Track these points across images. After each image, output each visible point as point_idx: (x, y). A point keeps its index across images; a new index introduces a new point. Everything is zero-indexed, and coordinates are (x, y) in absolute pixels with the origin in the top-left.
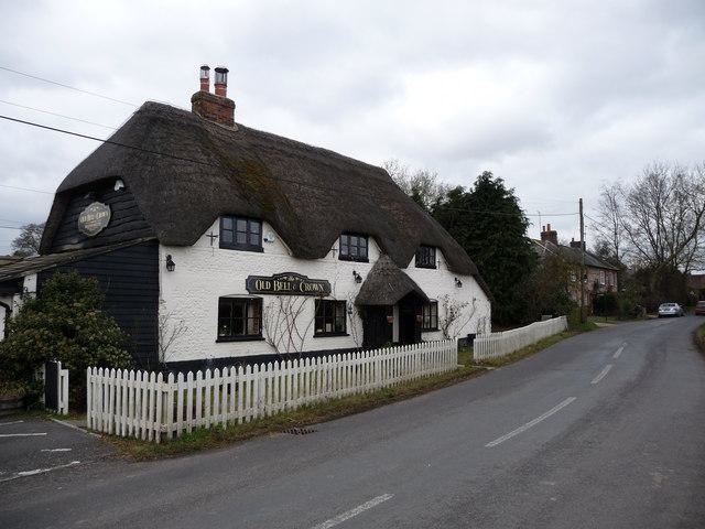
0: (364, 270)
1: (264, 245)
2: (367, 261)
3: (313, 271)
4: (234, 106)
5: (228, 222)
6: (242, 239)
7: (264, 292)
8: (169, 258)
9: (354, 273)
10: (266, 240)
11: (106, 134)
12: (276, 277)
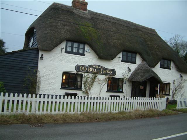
0: (133, 67)
1: (85, 53)
2: (135, 63)
3: (108, 65)
4: (87, 4)
5: (125, 53)
6: (166, 66)
7: (85, 72)
8: (42, 55)
9: (128, 68)
10: (86, 51)
11: (40, 14)
12: (90, 66)
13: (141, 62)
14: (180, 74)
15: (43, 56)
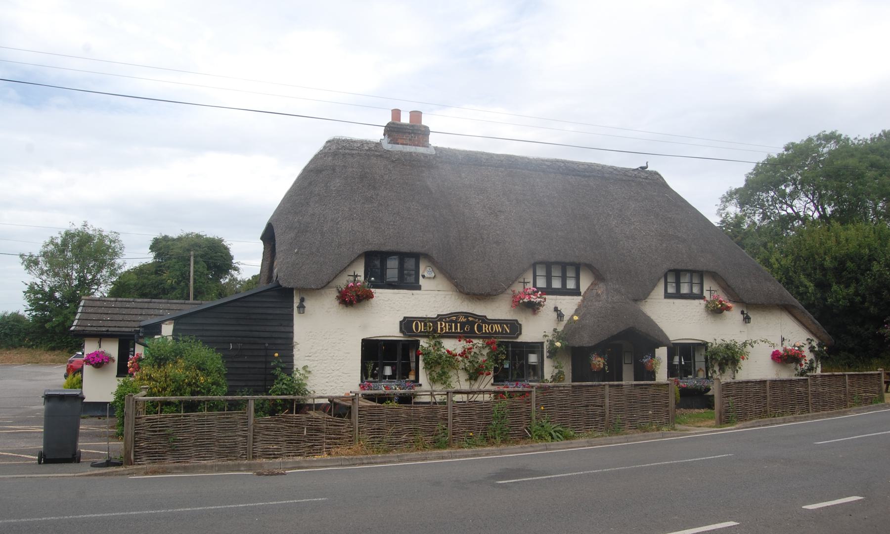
1: (422, 281)
7: (425, 335)
10: (424, 276)
12: (440, 318)
13: (594, 279)
14: (347, 276)
15: (305, 304)
